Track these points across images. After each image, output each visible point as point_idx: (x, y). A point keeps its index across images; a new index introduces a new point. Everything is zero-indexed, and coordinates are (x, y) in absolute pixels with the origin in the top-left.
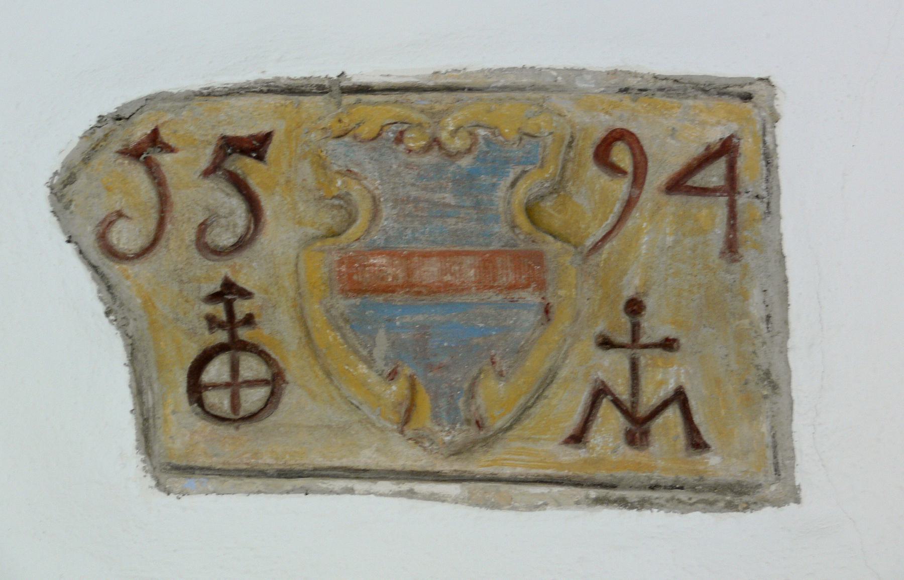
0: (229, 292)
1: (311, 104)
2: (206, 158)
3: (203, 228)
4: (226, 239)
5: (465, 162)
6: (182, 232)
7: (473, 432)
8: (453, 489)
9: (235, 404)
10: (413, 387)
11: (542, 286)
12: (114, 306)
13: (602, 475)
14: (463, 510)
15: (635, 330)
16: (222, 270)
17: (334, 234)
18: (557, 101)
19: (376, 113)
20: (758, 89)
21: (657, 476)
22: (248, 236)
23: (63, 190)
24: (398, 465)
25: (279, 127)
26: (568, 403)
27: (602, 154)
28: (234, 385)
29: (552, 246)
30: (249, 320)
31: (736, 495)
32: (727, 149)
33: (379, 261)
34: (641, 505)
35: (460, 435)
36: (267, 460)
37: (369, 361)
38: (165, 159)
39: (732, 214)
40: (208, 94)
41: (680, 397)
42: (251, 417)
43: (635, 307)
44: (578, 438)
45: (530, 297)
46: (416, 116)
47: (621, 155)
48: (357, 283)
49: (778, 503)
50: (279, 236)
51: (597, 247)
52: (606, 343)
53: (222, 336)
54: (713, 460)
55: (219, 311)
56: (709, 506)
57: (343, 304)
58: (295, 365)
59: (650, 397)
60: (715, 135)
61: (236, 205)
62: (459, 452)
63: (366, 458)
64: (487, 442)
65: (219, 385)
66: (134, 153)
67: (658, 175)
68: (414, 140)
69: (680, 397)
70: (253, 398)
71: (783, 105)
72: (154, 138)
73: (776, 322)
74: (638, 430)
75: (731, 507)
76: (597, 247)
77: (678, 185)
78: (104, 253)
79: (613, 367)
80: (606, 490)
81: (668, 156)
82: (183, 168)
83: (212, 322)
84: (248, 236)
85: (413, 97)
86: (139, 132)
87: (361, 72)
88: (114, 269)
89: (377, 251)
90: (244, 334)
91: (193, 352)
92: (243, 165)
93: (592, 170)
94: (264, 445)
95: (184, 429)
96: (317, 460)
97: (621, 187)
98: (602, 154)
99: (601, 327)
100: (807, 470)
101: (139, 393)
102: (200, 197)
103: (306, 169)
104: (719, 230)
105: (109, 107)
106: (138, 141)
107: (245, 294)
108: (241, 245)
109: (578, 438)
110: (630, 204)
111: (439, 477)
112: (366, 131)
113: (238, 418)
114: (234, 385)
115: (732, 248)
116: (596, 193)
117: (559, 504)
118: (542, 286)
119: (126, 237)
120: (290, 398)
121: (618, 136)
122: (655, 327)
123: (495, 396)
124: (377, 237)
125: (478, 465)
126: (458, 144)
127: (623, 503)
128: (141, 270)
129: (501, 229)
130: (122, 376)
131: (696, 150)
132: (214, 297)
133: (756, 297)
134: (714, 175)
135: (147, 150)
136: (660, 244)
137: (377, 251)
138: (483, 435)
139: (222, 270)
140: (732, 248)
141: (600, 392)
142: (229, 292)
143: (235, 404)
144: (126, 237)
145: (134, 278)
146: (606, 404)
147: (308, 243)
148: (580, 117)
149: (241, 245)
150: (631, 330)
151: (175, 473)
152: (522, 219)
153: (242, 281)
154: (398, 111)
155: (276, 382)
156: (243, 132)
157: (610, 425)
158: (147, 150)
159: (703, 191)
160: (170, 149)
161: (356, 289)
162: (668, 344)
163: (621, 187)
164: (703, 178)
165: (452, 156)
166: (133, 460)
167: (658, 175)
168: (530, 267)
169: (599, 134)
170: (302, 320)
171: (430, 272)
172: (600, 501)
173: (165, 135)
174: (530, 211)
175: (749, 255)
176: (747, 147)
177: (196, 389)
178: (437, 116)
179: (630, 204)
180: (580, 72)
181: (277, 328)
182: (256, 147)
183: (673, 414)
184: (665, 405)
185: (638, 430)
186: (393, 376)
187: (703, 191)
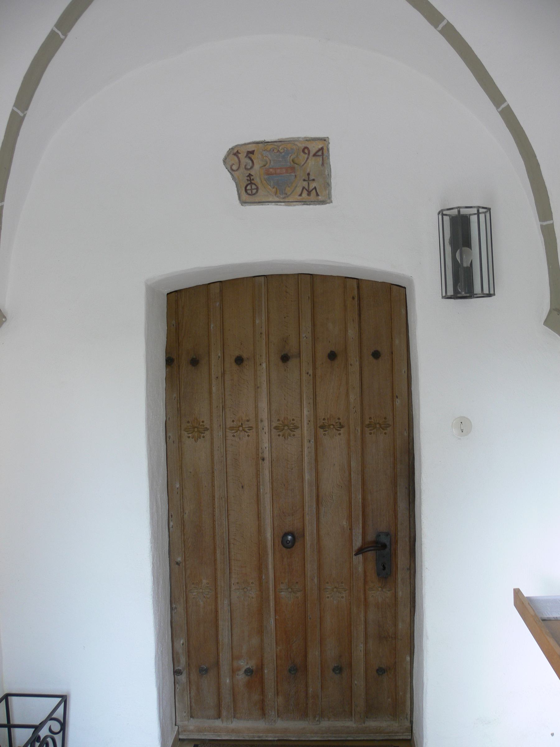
0: (250, 175)
1: (260, 145)
2: (245, 154)
3: (245, 166)
4: (249, 167)
5: (283, 154)
6: (243, 166)
7: (285, 195)
8: (283, 204)
9: (252, 192)
10: (277, 189)
11: (295, 172)
12: (234, 178)
13: (304, 200)
14: (285, 207)
15: (309, 178)
16: (249, 172)
17: (265, 166)
18: (296, 143)
19: (270, 147)
20: (327, 139)
21: (312, 200)
22: (372, 548)
23: (225, 161)
24: (275, 200)
25: (256, 149)
26: (299, 190)
27: (303, 151)
28: (251, 189)
29: (296, 166)
30: (253, 179)
31: (323, 202)
32: (322, 149)
33: (271, 170)
34: (310, 205)
35: (284, 196)
36: (257, 201)
37: (270, 186)
38: (239, 155)
39: (323, 159)
40: (245, 144)
41: (315, 188)
42: (254, 194)
43: (309, 174)
44: (300, 195)
45: (293, 174)
46: (276, 147)
47: (306, 151)
48: (268, 173)
49: (329, 203)
50: (257, 167)
51: (303, 165)
52: (304, 180)
53: (249, 182)
54: (320, 197)
55: (249, 178)
56: (319, 204)
57: (266, 177)
58: (260, 186)
59: (311, 188)
60: (320, 147)
61: (250, 162)
62: (284, 198)
63: (271, 200)
64: (288, 197)
65: (250, 190)
66: (235, 154)
67: (312, 153)
68: (275, 151)
69: (315, 188)
70: (254, 191)
71: (330, 141)
72: (238, 152)
73: (329, 175)
74: (309, 193)
75: (322, 204)
76: (303, 165)
77: (315, 155)
78: (231, 170)
79: (305, 184)
80: (305, 203)
81: (313, 151)
82: (242, 156)
83: (248, 180)
84: (372, 548)
85: (275, 143)
86: (235, 151)
87: (268, 139)
88: (233, 173)
89: (270, 168)
90: (252, 182)
91: (245, 185)
92: (251, 155)
93: (302, 153)
94: (257, 199)
95: (245, 196)
96: (264, 200)
97: (306, 156)
98: (303, 151)
99: (303, 178)
100: (333, 198)
101: (238, 191)
102: (245, 161)
103: (260, 156)
104: (321, 162)
105: (231, 147)
106: (234, 152)
107: (252, 176)
108: (252, 168)
109: (300, 195)
110: (308, 158)
111: (281, 202)
112: (268, 149)
113: (252, 194)
114: (251, 189)
115: (323, 164)
116: (303, 157)
117: (298, 205)
118: (295, 172)
119: (234, 167)
120: (260, 191)
121: (306, 148)
122: (312, 177)
123: (288, 190)
124: (271, 166)
125: (287, 200)
126: (282, 151)
127: (307, 204)
128: (237, 173)
129: (289, 164)
130: (236, 189)
131: (317, 149)
132: (248, 176)
133: (326, 172)
134: (320, 153)
135: (236, 154)
136: (312, 164)
137: (270, 168)
138: (287, 196)
139: (249, 172)
140: (323, 164)
141: (304, 188)
142: (250, 175)
143: (252, 192)
144: (234, 167)
145: (236, 174)
146: (304, 190)
147: (261, 167)
148: (299, 145)
149: (252, 168)
150: (308, 178)
151: (243, 203)
152: (292, 162)
153: (251, 173)
154: (272, 146)
155: (257, 189)
156: (250, 150)
157: (305, 194)
158: (236, 154)
159: (319, 156)
160: (240, 153)
161: (268, 174)
162: (313, 180)
163: (306, 156)
164: (318, 154)
165: (281, 153)
166: (238, 202)
167: (312, 153)
168: (293, 169)
169: (303, 148)
170: (260, 179)
171: (278, 171)
172: (304, 204)
173: (239, 151)
174: (293, 161)
175: (325, 165)
176: (325, 148)
177: (246, 190)
178: (279, 147)
179: (308, 158)
180: (300, 138)
181: (257, 180)
182: (252, 152)
183: (314, 191)
184: (313, 189)
185: (309, 193)
186: (274, 188)
187: (319, 156)
